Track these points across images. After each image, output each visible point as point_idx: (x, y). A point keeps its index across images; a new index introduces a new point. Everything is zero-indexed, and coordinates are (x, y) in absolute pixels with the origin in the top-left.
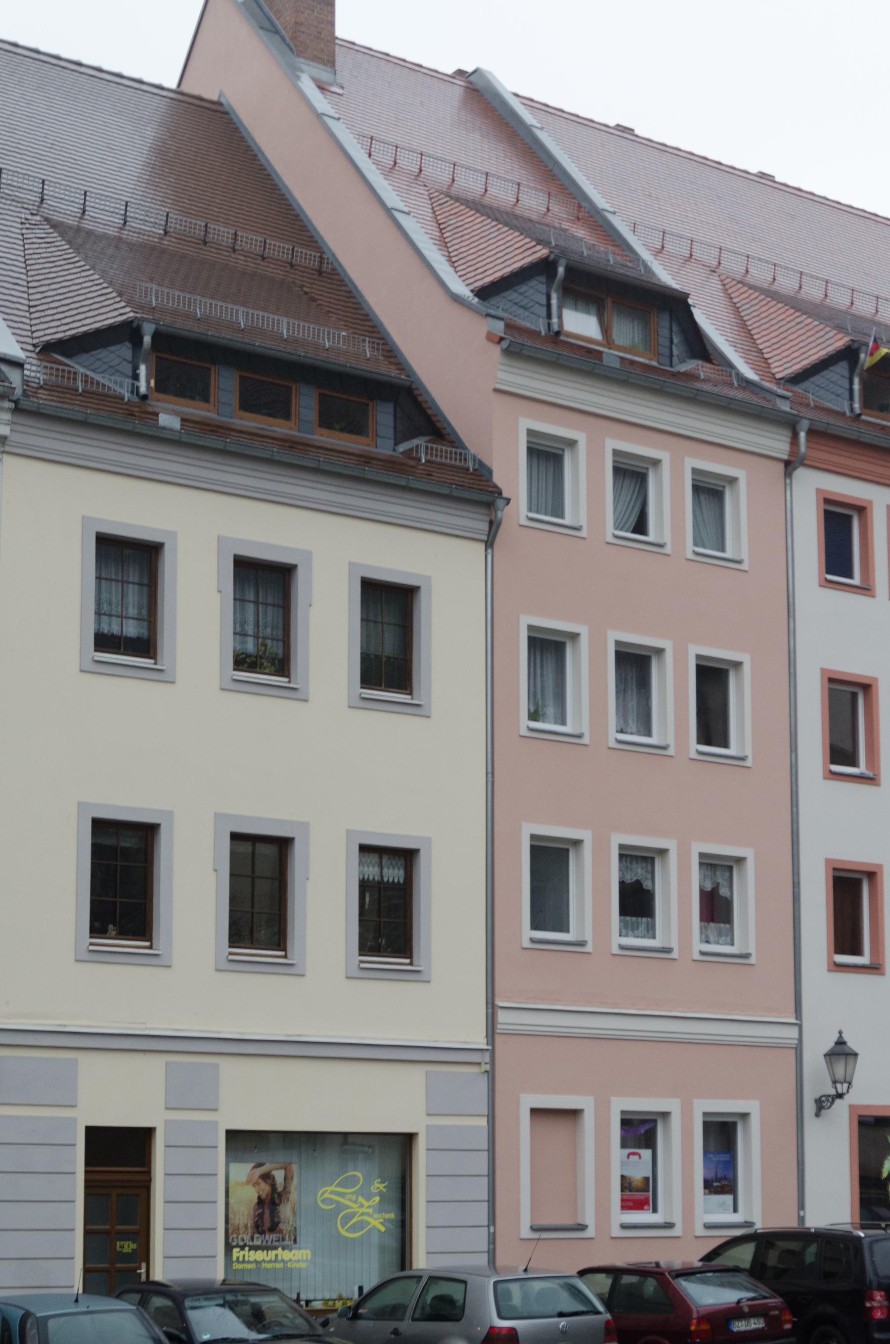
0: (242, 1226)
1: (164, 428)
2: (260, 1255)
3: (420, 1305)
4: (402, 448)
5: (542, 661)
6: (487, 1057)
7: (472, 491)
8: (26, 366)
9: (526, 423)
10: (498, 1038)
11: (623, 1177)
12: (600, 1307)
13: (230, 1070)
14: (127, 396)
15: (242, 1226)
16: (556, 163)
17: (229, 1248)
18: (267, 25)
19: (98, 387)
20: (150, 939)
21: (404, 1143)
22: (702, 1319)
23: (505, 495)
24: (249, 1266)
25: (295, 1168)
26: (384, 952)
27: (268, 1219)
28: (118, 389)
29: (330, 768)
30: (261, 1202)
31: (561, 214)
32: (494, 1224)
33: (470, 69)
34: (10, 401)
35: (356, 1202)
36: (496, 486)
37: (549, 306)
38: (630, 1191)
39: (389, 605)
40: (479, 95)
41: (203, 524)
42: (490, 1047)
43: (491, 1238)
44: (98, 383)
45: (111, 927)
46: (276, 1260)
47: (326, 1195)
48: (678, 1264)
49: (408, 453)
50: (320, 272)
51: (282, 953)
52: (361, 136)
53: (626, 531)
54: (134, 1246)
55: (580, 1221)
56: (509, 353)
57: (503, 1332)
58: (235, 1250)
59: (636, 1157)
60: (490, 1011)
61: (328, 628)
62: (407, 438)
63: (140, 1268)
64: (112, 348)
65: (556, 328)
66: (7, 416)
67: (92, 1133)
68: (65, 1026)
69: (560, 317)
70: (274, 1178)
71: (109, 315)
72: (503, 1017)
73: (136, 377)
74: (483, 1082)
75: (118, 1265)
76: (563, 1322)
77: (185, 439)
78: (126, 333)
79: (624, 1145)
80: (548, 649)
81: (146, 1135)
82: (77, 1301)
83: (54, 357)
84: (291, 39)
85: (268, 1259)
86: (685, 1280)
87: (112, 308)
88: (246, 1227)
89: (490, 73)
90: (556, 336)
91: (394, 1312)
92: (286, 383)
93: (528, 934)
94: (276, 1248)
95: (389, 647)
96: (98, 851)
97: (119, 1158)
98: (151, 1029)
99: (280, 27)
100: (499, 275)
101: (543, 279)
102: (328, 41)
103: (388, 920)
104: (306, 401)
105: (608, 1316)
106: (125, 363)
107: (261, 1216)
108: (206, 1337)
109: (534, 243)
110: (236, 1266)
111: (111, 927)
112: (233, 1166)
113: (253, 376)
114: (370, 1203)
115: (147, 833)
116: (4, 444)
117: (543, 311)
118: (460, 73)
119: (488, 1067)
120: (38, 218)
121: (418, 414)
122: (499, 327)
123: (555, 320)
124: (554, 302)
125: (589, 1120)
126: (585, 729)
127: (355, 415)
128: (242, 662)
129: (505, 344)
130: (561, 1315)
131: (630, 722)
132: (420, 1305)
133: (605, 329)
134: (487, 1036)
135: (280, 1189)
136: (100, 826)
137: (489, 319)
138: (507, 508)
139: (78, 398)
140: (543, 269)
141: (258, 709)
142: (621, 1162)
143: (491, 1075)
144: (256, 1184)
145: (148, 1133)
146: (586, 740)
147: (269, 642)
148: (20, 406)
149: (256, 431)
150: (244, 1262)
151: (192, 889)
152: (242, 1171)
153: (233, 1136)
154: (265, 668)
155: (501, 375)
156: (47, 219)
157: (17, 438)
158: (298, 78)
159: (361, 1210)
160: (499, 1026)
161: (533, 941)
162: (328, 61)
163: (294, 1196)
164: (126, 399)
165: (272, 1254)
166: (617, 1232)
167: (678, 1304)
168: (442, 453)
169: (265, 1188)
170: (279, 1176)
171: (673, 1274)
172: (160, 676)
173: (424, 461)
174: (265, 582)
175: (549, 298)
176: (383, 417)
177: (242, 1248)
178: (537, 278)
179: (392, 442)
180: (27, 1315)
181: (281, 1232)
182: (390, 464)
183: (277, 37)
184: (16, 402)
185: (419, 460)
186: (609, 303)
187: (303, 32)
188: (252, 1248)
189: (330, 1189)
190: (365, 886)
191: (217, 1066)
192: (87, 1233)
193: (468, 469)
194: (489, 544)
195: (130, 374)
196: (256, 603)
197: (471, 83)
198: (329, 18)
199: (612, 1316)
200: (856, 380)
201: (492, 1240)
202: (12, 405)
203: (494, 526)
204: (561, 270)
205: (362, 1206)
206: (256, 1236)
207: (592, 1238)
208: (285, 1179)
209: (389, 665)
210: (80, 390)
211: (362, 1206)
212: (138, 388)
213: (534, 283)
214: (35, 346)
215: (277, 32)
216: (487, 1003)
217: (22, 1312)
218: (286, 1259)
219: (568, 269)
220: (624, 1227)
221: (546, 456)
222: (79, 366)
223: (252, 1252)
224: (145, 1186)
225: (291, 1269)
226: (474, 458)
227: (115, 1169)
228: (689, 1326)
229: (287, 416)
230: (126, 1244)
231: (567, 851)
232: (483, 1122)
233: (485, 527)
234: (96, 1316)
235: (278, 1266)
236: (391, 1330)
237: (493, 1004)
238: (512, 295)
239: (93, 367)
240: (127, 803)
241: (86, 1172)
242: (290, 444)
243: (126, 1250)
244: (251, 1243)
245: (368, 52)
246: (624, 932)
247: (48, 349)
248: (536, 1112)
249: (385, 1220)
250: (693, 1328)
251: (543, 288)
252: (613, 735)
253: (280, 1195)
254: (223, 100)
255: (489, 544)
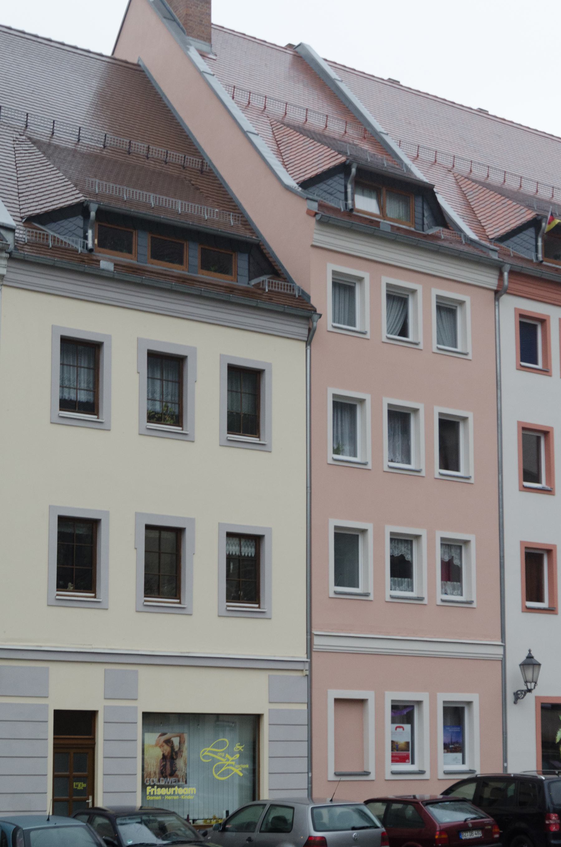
0: (152, 773)
1: (103, 270)
2: (164, 791)
3: (265, 822)
4: (253, 282)
5: (341, 416)
6: (307, 666)
7: (297, 309)
8: (17, 231)
9: (331, 267)
10: (314, 654)
11: (393, 742)
12: (378, 824)
13: (145, 674)
14: (80, 249)
15: (152, 773)
16: (351, 103)
17: (144, 786)
18: (168, 16)
19: (62, 244)
20: (94, 592)
21: (255, 720)
22: (443, 831)
23: (318, 312)
24: (157, 798)
25: (186, 736)
26: (242, 600)
27: (169, 768)
28: (75, 245)
29: (208, 484)
30: (164, 757)
31: (354, 135)
32: (311, 772)
33: (296, 44)
34: (6, 252)
35: (224, 757)
36: (312, 307)
37: (346, 193)
38: (397, 751)
39: (245, 381)
40: (302, 60)
41: (128, 330)
42: (309, 660)
43: (310, 780)
44: (62, 241)
45: (70, 584)
46: (174, 794)
47: (206, 753)
48: (427, 797)
49: (257, 286)
50: (202, 172)
51: (178, 601)
52: (227, 86)
53: (395, 335)
54: (84, 785)
55: (366, 770)
56: (321, 222)
57: (317, 840)
58: (148, 788)
59: (401, 729)
60: (309, 637)
61: (207, 396)
62: (257, 276)
63: (88, 799)
64: (71, 220)
65: (350, 206)
66: (5, 262)
67: (58, 714)
68: (41, 646)
69: (353, 200)
70: (172, 742)
71: (69, 199)
72: (317, 641)
73: (86, 238)
74: (305, 682)
75: (74, 797)
76: (355, 833)
77: (117, 276)
78: (80, 210)
79: (393, 722)
80: (345, 409)
81: (92, 715)
82: (48, 820)
83: (34, 225)
84: (184, 24)
85: (169, 793)
86: (432, 807)
87: (70, 194)
88: (155, 773)
89: (309, 46)
90: (351, 212)
91: (248, 827)
92: (180, 242)
93: (333, 588)
94: (174, 787)
95: (245, 408)
96: (61, 536)
97: (75, 730)
98: (95, 648)
99: (176, 17)
100: (314, 173)
101: (342, 176)
102: (207, 26)
103: (244, 580)
104: (193, 253)
105: (383, 830)
106: (79, 229)
107: (164, 766)
108: (130, 843)
109: (336, 153)
110: (149, 798)
111: (70, 584)
112: (147, 735)
113: (159, 237)
114: (233, 758)
115: (93, 525)
116: (2, 279)
117: (342, 196)
118: (290, 46)
119: (307, 673)
120: (24, 137)
121: (263, 261)
122: (314, 206)
123: (350, 202)
124: (349, 190)
125: (371, 706)
126: (369, 460)
127: (224, 261)
128: (153, 417)
129: (318, 217)
130: (354, 829)
131: (397, 455)
132: (265, 822)
133: (382, 208)
134: (307, 653)
135: (176, 749)
136: (63, 521)
137: (308, 201)
138: (319, 320)
139: (49, 251)
140: (342, 169)
141: (163, 447)
142: (392, 732)
143: (309, 678)
144: (161, 746)
145: (93, 714)
146: (369, 466)
147: (169, 405)
148: (12, 256)
149: (161, 272)
150: (154, 795)
151: (121, 560)
152: (153, 738)
153: (147, 716)
154: (167, 421)
155: (316, 236)
156: (29, 138)
157: (11, 276)
158: (188, 49)
159: (228, 763)
160: (314, 647)
161: (336, 593)
162: (207, 38)
163: (185, 754)
164: (80, 252)
165: (171, 790)
166: (389, 776)
167: (427, 822)
168: (279, 285)
169: (167, 749)
170: (176, 741)
171: (424, 803)
172: (101, 426)
173: (267, 290)
174: (167, 367)
175: (346, 188)
176: (242, 263)
177: (153, 786)
178: (339, 175)
179: (247, 278)
180: (17, 829)
181: (177, 776)
182: (246, 293)
183: (175, 23)
184: (10, 253)
185: (264, 290)
186: (384, 191)
187: (191, 20)
188: (159, 786)
189: (208, 749)
190: (230, 558)
191: (137, 672)
192: (55, 777)
193: (295, 296)
194: (308, 343)
195: (82, 236)
196: (162, 380)
197: (297, 52)
198: (207, 12)
199: (386, 829)
200: (540, 240)
201: (310, 781)
202: (8, 255)
203: (311, 331)
204: (354, 170)
205: (228, 760)
206: (161, 779)
207: (373, 780)
208: (180, 743)
209: (245, 419)
210: (51, 246)
211: (228, 760)
212: (87, 244)
213: (336, 178)
214: (22, 218)
215: (175, 20)
216: (307, 632)
217: (14, 827)
218: (180, 793)
219: (358, 170)
220: (393, 773)
221: (344, 288)
222: (50, 231)
223: (159, 789)
224: (91, 747)
225: (183, 800)
226: (299, 289)
227: (72, 737)
228: (434, 836)
229: (181, 262)
230: (79, 784)
231: (357, 536)
232: (305, 707)
233: (306, 332)
234: (61, 829)
235: (175, 798)
236: (247, 838)
237: (311, 633)
238: (323, 186)
239: (59, 231)
240: (80, 506)
241: (54, 738)
242: (183, 280)
243: (79, 788)
244: (158, 784)
245: (232, 33)
246: (393, 587)
247: (30, 220)
248: (338, 701)
249: (243, 769)
250: (437, 837)
251: (342, 182)
252: (386, 463)
253: (176, 753)
254: (140, 63)
255: (308, 343)
